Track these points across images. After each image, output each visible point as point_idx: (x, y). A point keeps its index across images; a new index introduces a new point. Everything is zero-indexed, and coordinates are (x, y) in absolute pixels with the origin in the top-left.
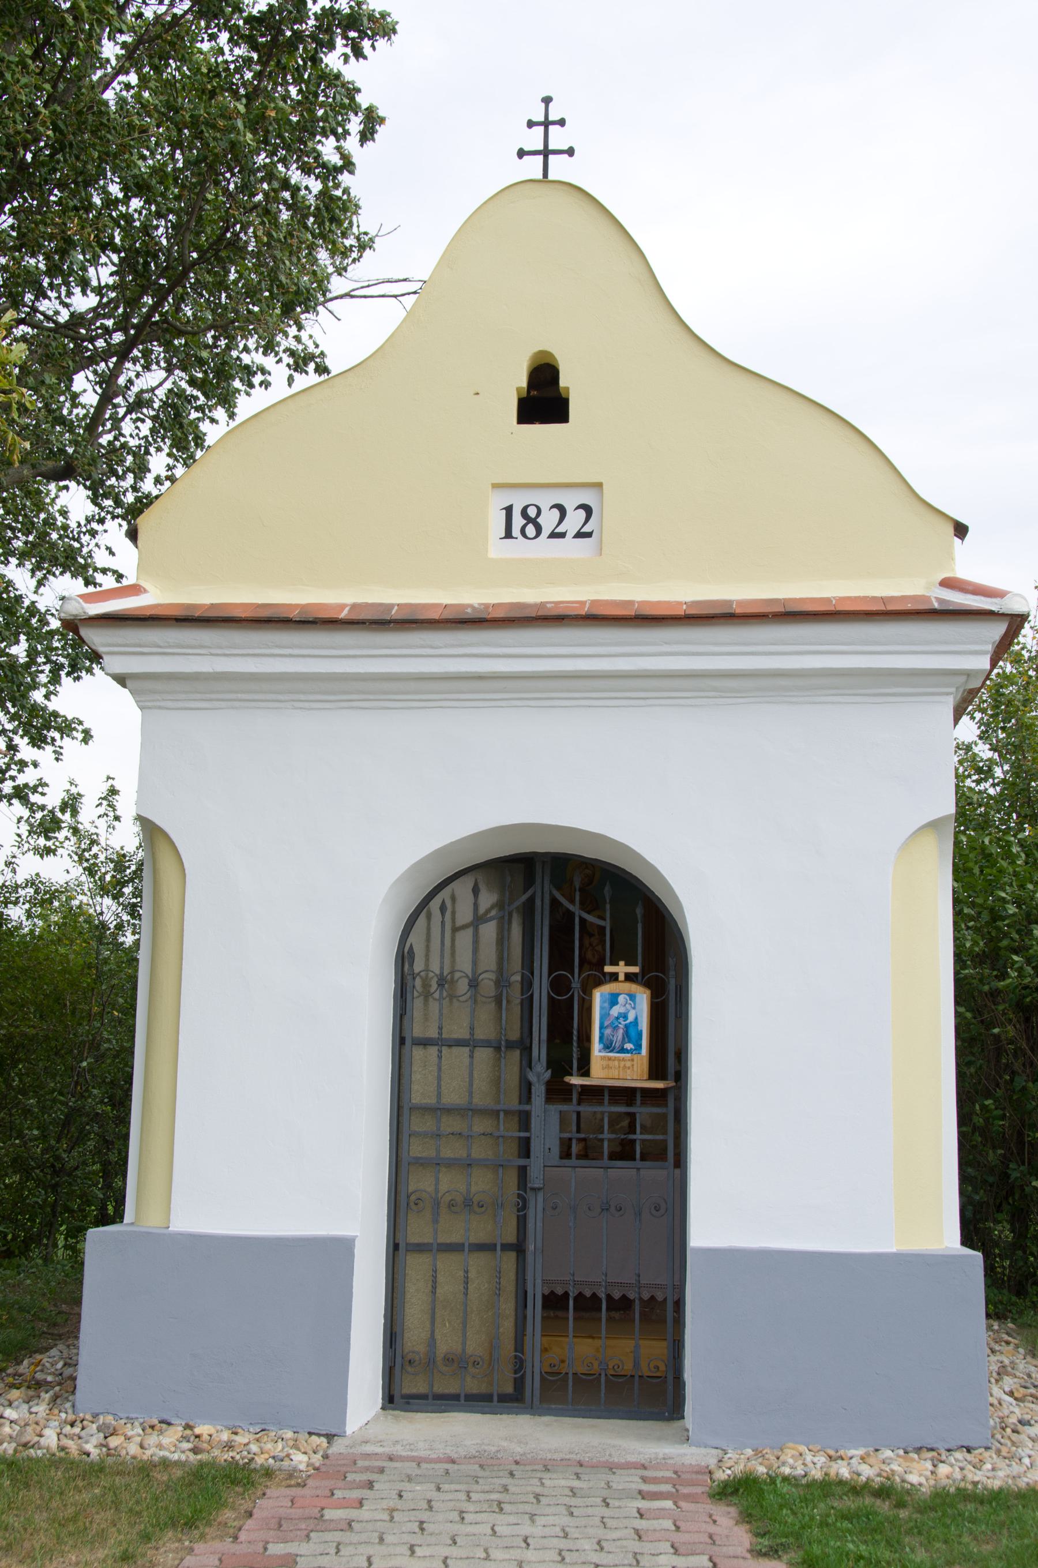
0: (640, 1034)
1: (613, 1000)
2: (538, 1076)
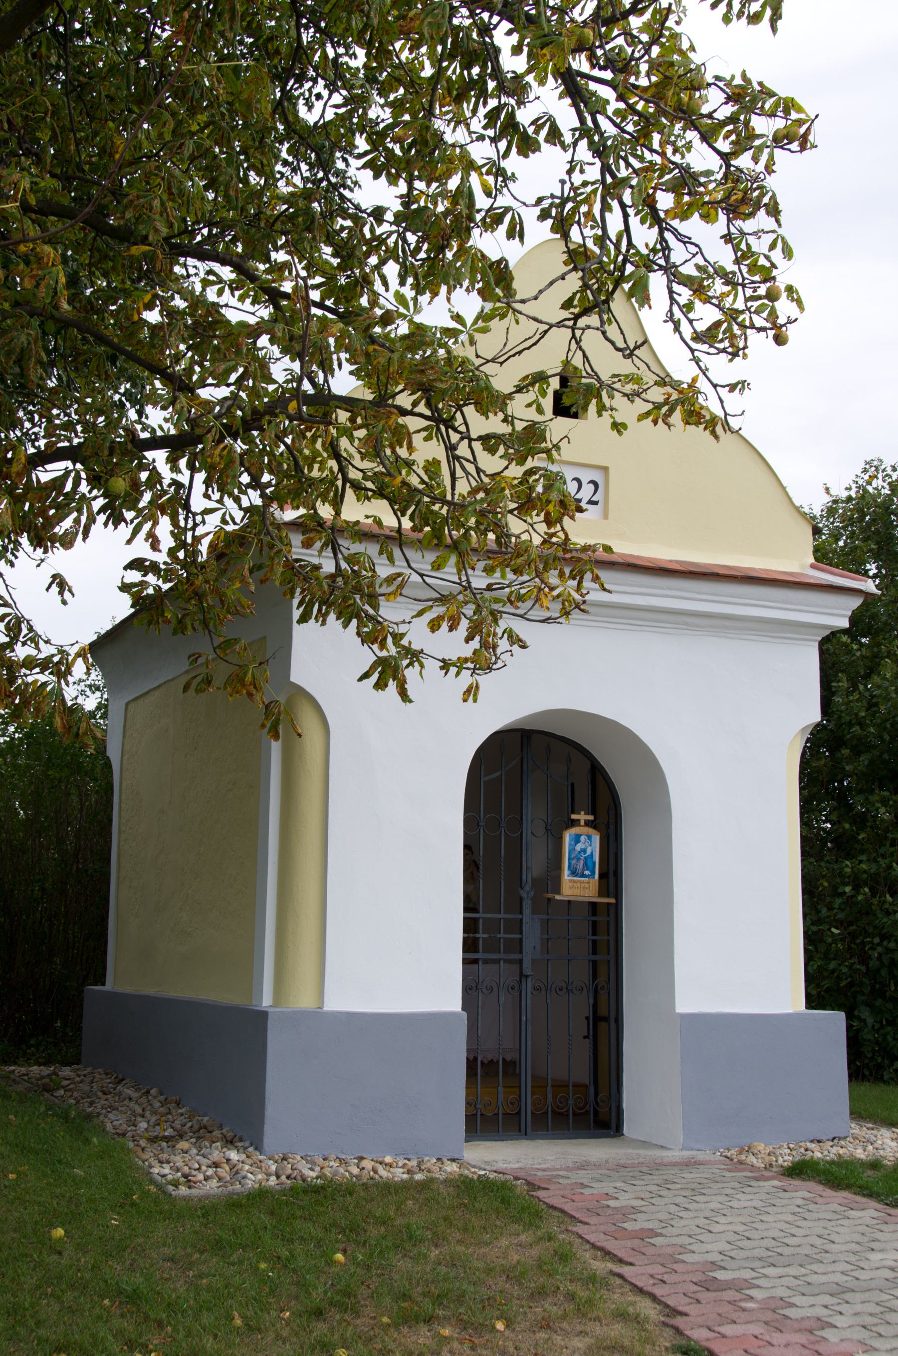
0: (594, 863)
1: (577, 839)
2: (528, 893)
